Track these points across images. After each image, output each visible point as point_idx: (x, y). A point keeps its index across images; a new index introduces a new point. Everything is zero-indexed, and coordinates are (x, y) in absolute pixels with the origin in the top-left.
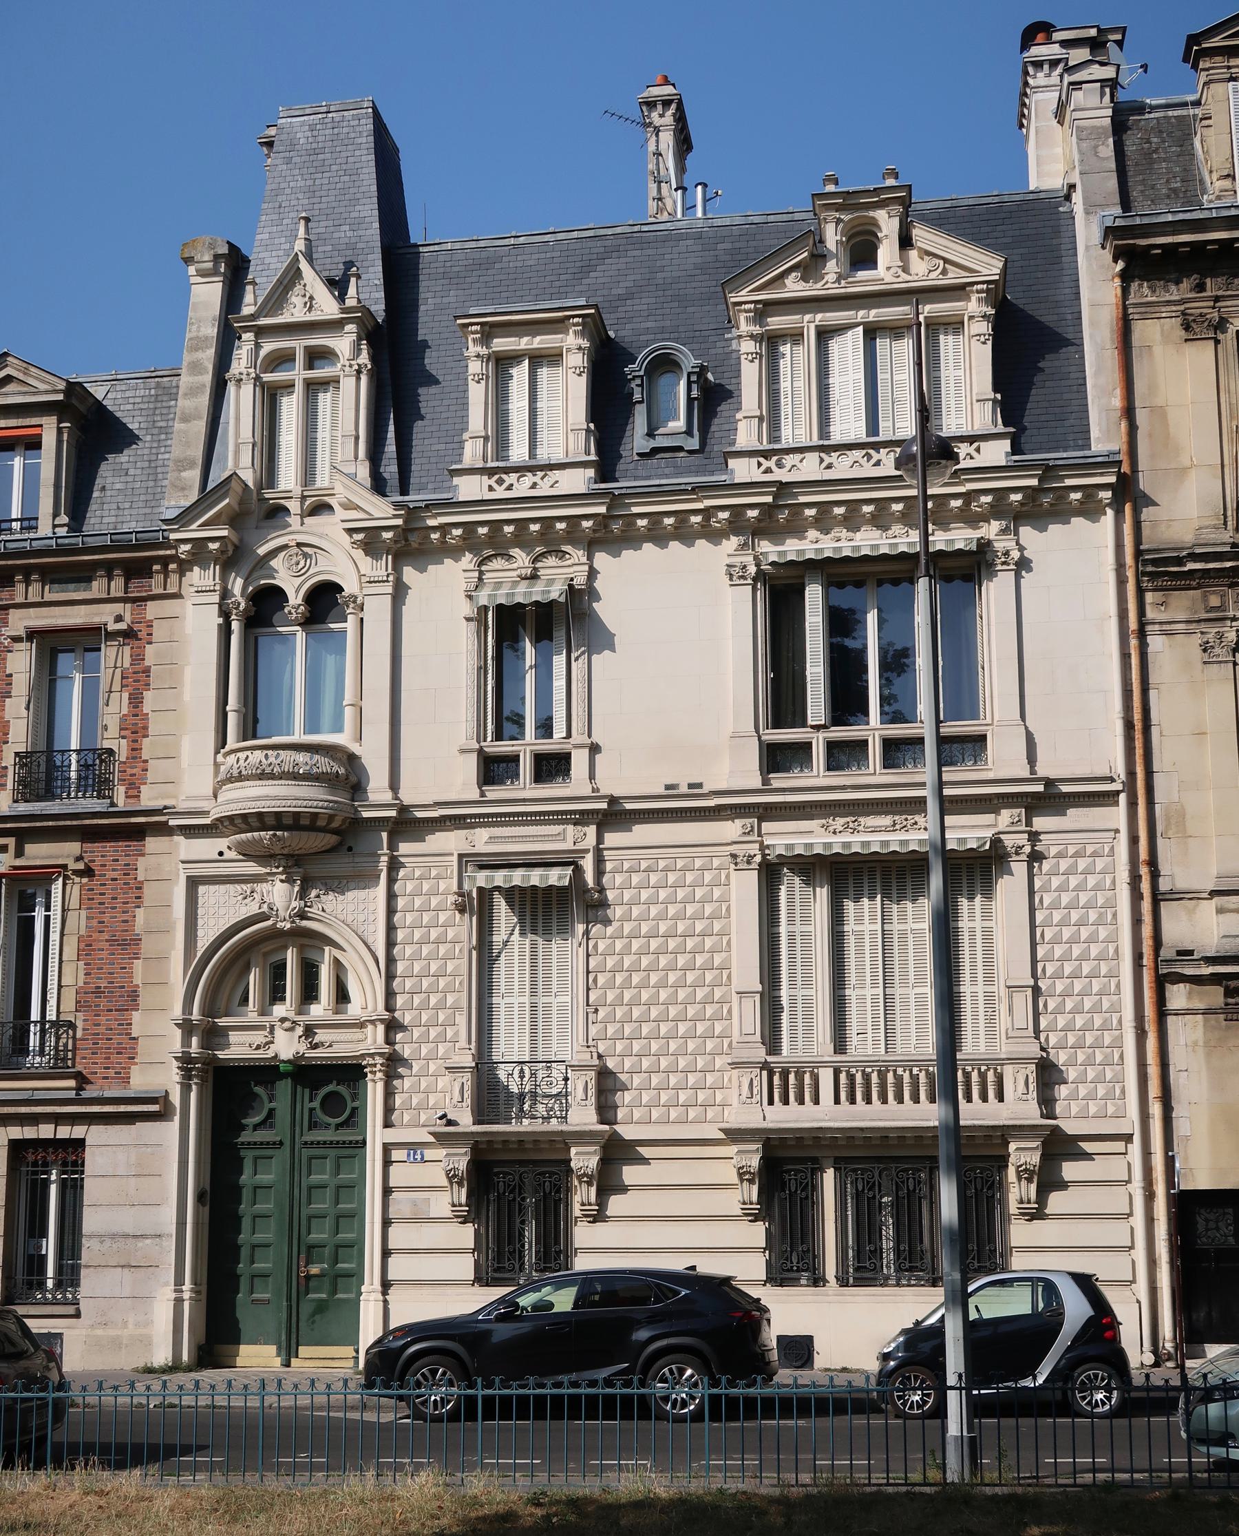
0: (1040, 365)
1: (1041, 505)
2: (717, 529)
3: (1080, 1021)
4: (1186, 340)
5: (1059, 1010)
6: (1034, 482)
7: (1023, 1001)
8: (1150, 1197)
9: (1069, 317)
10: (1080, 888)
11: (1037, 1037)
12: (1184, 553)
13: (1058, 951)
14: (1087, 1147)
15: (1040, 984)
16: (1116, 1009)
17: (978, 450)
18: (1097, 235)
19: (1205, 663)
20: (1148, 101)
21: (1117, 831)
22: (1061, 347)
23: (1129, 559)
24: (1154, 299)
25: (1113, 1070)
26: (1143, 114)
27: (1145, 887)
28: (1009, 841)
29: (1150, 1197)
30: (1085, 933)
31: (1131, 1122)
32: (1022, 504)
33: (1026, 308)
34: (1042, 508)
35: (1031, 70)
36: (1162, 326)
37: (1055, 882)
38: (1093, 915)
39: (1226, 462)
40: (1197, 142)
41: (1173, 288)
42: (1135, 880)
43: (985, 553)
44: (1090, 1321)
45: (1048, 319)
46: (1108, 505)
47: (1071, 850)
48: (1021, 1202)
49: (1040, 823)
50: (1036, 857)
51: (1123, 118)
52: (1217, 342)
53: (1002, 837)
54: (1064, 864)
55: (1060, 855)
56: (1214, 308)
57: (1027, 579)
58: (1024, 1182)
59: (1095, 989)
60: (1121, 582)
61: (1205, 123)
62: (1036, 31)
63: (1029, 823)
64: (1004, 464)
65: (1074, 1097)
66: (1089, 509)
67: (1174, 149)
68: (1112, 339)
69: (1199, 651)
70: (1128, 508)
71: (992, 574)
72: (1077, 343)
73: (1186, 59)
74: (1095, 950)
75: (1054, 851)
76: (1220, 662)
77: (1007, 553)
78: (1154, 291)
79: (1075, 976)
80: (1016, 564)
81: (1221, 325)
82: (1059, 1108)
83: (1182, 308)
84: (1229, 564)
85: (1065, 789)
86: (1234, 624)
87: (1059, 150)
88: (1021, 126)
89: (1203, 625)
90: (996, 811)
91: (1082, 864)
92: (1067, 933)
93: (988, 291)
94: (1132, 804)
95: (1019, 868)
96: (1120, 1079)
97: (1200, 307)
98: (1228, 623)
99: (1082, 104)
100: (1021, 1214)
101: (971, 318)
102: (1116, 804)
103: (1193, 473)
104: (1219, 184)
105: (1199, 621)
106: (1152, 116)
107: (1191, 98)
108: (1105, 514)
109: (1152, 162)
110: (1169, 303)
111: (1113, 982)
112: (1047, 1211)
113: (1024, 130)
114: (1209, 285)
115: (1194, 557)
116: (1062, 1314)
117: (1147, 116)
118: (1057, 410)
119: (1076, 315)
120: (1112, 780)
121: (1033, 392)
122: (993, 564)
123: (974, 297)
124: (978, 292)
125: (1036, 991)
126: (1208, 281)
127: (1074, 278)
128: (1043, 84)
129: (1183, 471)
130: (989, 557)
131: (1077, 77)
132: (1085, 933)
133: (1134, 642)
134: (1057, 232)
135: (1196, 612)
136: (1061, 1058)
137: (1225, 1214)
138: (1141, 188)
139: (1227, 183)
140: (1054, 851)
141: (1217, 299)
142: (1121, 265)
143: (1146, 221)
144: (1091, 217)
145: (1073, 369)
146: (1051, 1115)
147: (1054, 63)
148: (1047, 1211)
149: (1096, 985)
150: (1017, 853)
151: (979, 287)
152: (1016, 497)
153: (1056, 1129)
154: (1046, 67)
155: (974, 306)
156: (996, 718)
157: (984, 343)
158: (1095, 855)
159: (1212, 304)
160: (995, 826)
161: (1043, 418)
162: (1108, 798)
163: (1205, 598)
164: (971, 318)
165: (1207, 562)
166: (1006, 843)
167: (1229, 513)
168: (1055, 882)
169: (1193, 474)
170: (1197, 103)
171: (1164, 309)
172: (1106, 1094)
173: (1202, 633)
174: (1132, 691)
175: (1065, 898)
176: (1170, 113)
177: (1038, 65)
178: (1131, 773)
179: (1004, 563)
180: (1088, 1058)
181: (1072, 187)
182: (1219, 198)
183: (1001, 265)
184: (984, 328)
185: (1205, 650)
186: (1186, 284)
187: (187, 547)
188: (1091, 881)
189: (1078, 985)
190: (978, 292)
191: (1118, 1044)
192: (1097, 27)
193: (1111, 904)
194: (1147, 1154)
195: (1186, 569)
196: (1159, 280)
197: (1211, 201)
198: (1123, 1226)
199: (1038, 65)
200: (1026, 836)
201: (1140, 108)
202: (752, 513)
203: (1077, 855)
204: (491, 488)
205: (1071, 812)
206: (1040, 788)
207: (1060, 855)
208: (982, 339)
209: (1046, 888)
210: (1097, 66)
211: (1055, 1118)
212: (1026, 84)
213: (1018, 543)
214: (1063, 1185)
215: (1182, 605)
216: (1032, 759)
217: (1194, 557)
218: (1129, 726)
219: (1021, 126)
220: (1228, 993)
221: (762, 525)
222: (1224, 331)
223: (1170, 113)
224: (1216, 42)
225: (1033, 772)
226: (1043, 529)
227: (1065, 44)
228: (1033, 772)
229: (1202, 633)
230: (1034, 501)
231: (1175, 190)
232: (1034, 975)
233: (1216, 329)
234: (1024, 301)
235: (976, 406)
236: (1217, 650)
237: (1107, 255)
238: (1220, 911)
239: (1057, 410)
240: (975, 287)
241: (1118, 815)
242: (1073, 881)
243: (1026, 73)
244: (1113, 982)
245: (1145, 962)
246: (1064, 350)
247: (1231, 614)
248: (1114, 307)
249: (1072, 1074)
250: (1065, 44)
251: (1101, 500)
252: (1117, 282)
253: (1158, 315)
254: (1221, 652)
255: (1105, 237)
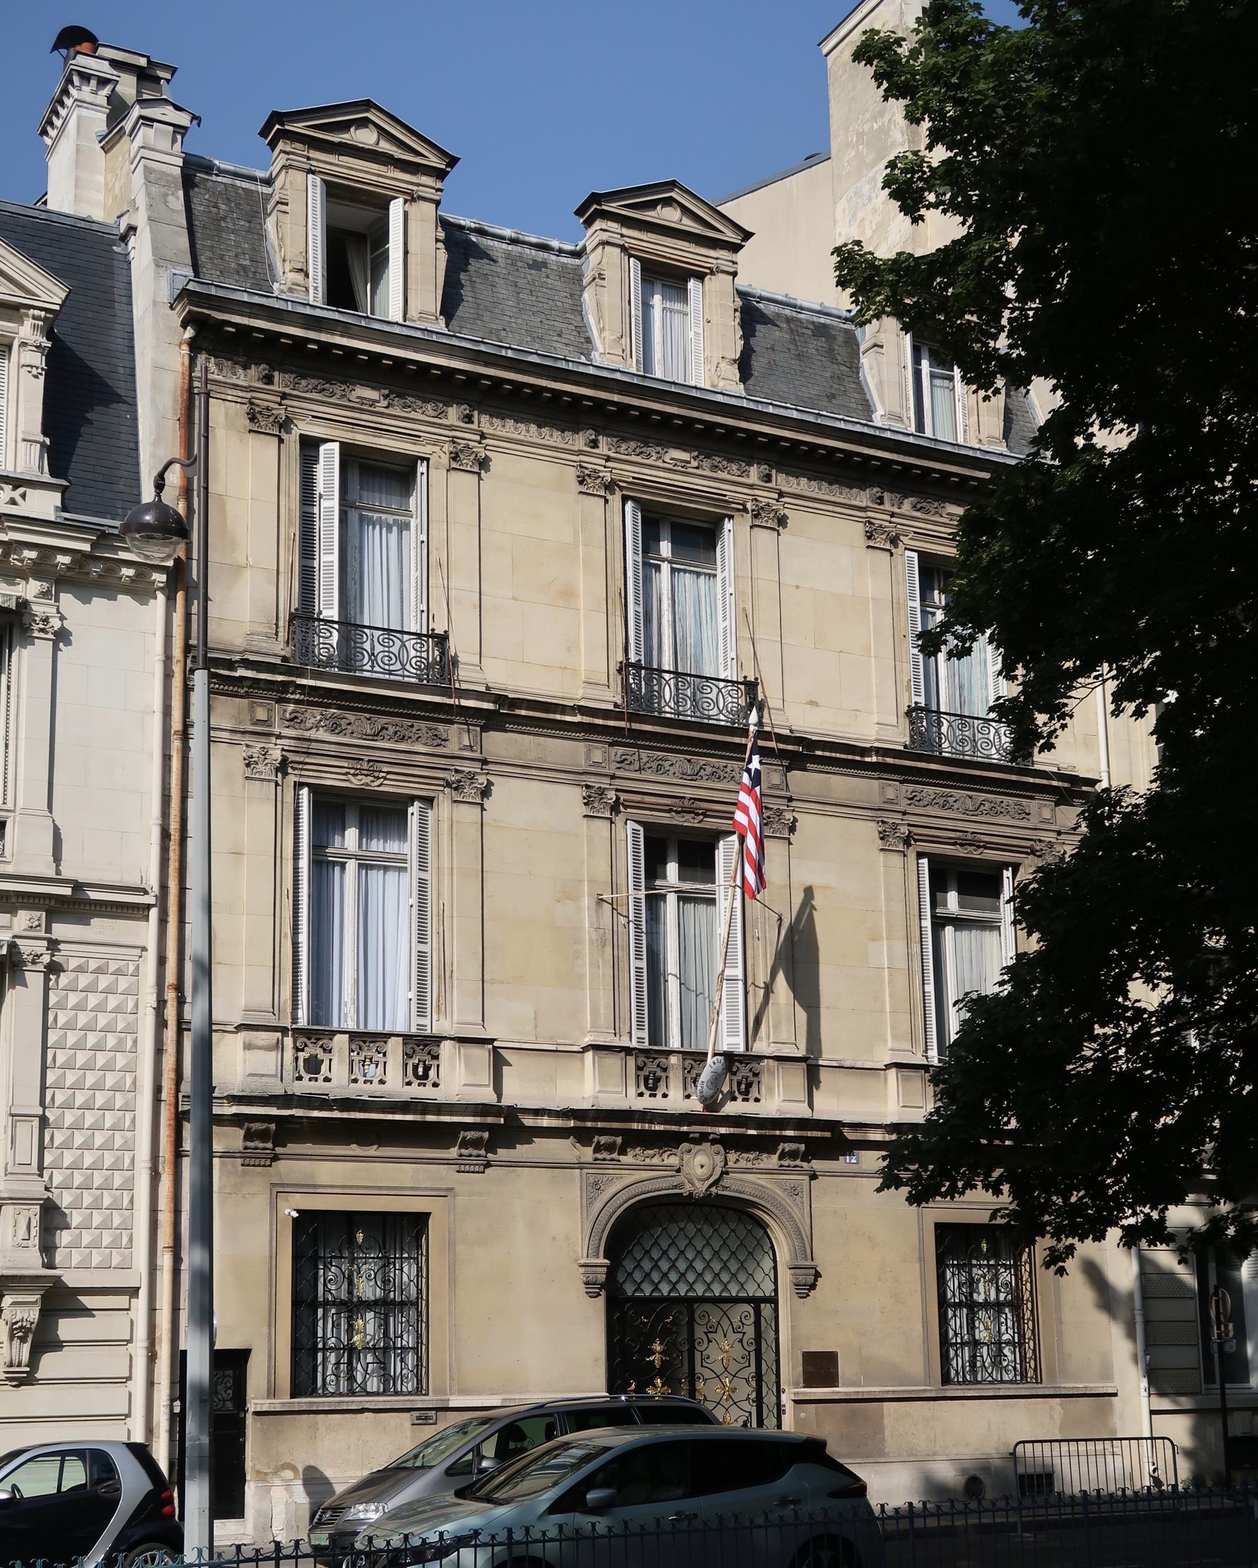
0: (89, 415)
1: (88, 573)
2: (15, 568)
3: (89, 1159)
4: (250, 431)
5: (67, 1145)
6: (86, 547)
7: (28, 1131)
8: (152, 1358)
9: (121, 370)
10: (100, 1008)
11: (41, 1175)
12: (237, 658)
13: (71, 1078)
14: (88, 1302)
15: (47, 1114)
16: (129, 1147)
17: (23, 496)
18: (165, 296)
19: (247, 778)
20: (217, 162)
21: (144, 949)
22: (112, 402)
23: (177, 652)
24: (220, 378)
25: (121, 1215)
26: (211, 174)
27: (170, 1013)
28: (26, 947)
29: (152, 1358)
30: (101, 1059)
31: (138, 1275)
32: (69, 568)
33: (74, 347)
34: (87, 577)
35: (76, 79)
36: (227, 410)
37: (73, 999)
38: (111, 1041)
39: (282, 569)
40: (270, 224)
41: (240, 371)
42: (161, 1003)
43: (22, 615)
44: (149, 1495)
45: (98, 366)
46: (161, 589)
47: (93, 965)
48: (11, 1365)
49: (61, 930)
50: (54, 969)
51: (193, 172)
52: (281, 441)
53: (18, 941)
54: (84, 980)
55: (80, 969)
56: (280, 404)
57: (65, 653)
58: (16, 1342)
59: (108, 1124)
60: (168, 676)
61: (283, 208)
62: (74, 38)
63: (48, 930)
64: (53, 519)
65: (75, 1245)
66: (140, 590)
67: (242, 223)
68: (174, 410)
69: (242, 764)
70: (180, 596)
71: (27, 639)
72: (133, 405)
73: (264, 133)
74: (111, 1080)
75: (73, 963)
76: (263, 780)
77: (46, 620)
78: (221, 370)
79: (87, 1107)
80: (55, 634)
81: (286, 425)
82: (59, 1257)
83: (249, 395)
84: (280, 678)
85: (94, 895)
86: (279, 741)
87: (100, 178)
88: (44, 132)
89: (247, 737)
90: (12, 911)
91: (104, 982)
92: (81, 1058)
93: (45, 319)
94: (163, 921)
95: (34, 979)
96: (127, 1226)
97: (266, 400)
98: (273, 740)
99: (152, 143)
100: (8, 1379)
101: (23, 344)
102: (147, 918)
103: (248, 572)
104: (292, 276)
105: (244, 733)
106: (220, 179)
107: (260, 174)
108: (156, 598)
109: (220, 230)
110: (235, 386)
111: (129, 1116)
112: (38, 1376)
113: (48, 141)
114: (276, 379)
115: (247, 664)
116: (119, 1489)
117: (214, 178)
118: (105, 471)
119: (128, 371)
120: (146, 892)
121: (80, 444)
122: (30, 629)
123: (29, 323)
124: (34, 318)
125: (44, 1121)
126: (276, 374)
127: (127, 329)
128: (88, 100)
129: (238, 569)
130: (26, 620)
131: (149, 112)
132: (101, 1059)
133: (176, 744)
134: (109, 272)
135: (240, 723)
136: (65, 1200)
137: (224, 1376)
138: (209, 254)
139: (299, 278)
140: (73, 963)
141: (284, 396)
142: (189, 333)
143: (221, 293)
144: (161, 271)
145: (124, 429)
146: (50, 1265)
147: (103, 82)
148: (38, 1376)
149: (110, 1119)
150: (34, 963)
151: (37, 312)
152: (64, 560)
153: (58, 1279)
154: (93, 82)
155: (27, 331)
156: (20, 804)
157: (36, 377)
158: (118, 972)
159: (278, 399)
160: (10, 928)
161: (90, 476)
162: (137, 912)
163: (251, 708)
164: (23, 344)
165: (258, 671)
166: (22, 949)
167: (281, 624)
168: (73, 999)
169: (248, 573)
170: (269, 182)
171: (230, 392)
172: (113, 1241)
173: (247, 746)
174: (169, 796)
175: (83, 1019)
176: (238, 183)
177: (86, 77)
178: (164, 887)
179: (41, 630)
180: (96, 1200)
181: (132, 229)
182: (291, 290)
183: (63, 295)
184: (38, 360)
185: (248, 765)
186: (254, 371)
187: (33, 554)
188: (113, 1002)
189: (90, 1118)
190: (34, 318)
191: (128, 1186)
192: (148, 57)
193: (131, 1030)
194: (152, 1309)
195: (237, 674)
196: (228, 359)
197: (282, 291)
198: (120, 1392)
199: (86, 77)
200: (45, 943)
201: (209, 168)
202: (64, 560)
203: (100, 971)
204: (13, 502)
205: (95, 922)
206: (67, 891)
207: (80, 969)
208: (34, 371)
209: (61, 1006)
210: (171, 108)
211: (55, 1268)
212: (65, 92)
213: (58, 612)
214: (57, 1345)
215: (229, 712)
216: (57, 857)
217: (247, 664)
218: (165, 835)
219: (44, 132)
220: (248, 1136)
221: (69, 574)
222: (289, 432)
223: (238, 183)
224: (298, 127)
225: (58, 872)
226: (86, 601)
227: (115, 63)
228: (58, 872)
229: (247, 746)
230: (81, 567)
231: (244, 268)
232: (42, 1103)
233: (281, 426)
234: (72, 339)
235: (22, 445)
236: (260, 767)
237: (176, 318)
238: (248, 1047)
239: (105, 471)
240: (31, 311)
241: (147, 931)
242: (93, 1000)
243: (70, 81)
244: (129, 1116)
245: (164, 1096)
246: (115, 406)
247: (277, 730)
248: (180, 376)
249: (76, 1218)
250: (115, 63)
251: (153, 582)
252: (185, 349)
253: (223, 396)
254: (266, 771)
255: (179, 298)
